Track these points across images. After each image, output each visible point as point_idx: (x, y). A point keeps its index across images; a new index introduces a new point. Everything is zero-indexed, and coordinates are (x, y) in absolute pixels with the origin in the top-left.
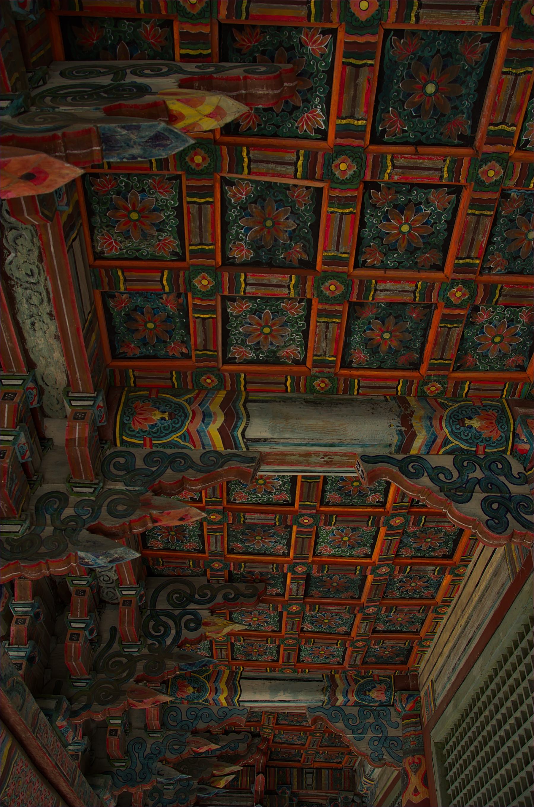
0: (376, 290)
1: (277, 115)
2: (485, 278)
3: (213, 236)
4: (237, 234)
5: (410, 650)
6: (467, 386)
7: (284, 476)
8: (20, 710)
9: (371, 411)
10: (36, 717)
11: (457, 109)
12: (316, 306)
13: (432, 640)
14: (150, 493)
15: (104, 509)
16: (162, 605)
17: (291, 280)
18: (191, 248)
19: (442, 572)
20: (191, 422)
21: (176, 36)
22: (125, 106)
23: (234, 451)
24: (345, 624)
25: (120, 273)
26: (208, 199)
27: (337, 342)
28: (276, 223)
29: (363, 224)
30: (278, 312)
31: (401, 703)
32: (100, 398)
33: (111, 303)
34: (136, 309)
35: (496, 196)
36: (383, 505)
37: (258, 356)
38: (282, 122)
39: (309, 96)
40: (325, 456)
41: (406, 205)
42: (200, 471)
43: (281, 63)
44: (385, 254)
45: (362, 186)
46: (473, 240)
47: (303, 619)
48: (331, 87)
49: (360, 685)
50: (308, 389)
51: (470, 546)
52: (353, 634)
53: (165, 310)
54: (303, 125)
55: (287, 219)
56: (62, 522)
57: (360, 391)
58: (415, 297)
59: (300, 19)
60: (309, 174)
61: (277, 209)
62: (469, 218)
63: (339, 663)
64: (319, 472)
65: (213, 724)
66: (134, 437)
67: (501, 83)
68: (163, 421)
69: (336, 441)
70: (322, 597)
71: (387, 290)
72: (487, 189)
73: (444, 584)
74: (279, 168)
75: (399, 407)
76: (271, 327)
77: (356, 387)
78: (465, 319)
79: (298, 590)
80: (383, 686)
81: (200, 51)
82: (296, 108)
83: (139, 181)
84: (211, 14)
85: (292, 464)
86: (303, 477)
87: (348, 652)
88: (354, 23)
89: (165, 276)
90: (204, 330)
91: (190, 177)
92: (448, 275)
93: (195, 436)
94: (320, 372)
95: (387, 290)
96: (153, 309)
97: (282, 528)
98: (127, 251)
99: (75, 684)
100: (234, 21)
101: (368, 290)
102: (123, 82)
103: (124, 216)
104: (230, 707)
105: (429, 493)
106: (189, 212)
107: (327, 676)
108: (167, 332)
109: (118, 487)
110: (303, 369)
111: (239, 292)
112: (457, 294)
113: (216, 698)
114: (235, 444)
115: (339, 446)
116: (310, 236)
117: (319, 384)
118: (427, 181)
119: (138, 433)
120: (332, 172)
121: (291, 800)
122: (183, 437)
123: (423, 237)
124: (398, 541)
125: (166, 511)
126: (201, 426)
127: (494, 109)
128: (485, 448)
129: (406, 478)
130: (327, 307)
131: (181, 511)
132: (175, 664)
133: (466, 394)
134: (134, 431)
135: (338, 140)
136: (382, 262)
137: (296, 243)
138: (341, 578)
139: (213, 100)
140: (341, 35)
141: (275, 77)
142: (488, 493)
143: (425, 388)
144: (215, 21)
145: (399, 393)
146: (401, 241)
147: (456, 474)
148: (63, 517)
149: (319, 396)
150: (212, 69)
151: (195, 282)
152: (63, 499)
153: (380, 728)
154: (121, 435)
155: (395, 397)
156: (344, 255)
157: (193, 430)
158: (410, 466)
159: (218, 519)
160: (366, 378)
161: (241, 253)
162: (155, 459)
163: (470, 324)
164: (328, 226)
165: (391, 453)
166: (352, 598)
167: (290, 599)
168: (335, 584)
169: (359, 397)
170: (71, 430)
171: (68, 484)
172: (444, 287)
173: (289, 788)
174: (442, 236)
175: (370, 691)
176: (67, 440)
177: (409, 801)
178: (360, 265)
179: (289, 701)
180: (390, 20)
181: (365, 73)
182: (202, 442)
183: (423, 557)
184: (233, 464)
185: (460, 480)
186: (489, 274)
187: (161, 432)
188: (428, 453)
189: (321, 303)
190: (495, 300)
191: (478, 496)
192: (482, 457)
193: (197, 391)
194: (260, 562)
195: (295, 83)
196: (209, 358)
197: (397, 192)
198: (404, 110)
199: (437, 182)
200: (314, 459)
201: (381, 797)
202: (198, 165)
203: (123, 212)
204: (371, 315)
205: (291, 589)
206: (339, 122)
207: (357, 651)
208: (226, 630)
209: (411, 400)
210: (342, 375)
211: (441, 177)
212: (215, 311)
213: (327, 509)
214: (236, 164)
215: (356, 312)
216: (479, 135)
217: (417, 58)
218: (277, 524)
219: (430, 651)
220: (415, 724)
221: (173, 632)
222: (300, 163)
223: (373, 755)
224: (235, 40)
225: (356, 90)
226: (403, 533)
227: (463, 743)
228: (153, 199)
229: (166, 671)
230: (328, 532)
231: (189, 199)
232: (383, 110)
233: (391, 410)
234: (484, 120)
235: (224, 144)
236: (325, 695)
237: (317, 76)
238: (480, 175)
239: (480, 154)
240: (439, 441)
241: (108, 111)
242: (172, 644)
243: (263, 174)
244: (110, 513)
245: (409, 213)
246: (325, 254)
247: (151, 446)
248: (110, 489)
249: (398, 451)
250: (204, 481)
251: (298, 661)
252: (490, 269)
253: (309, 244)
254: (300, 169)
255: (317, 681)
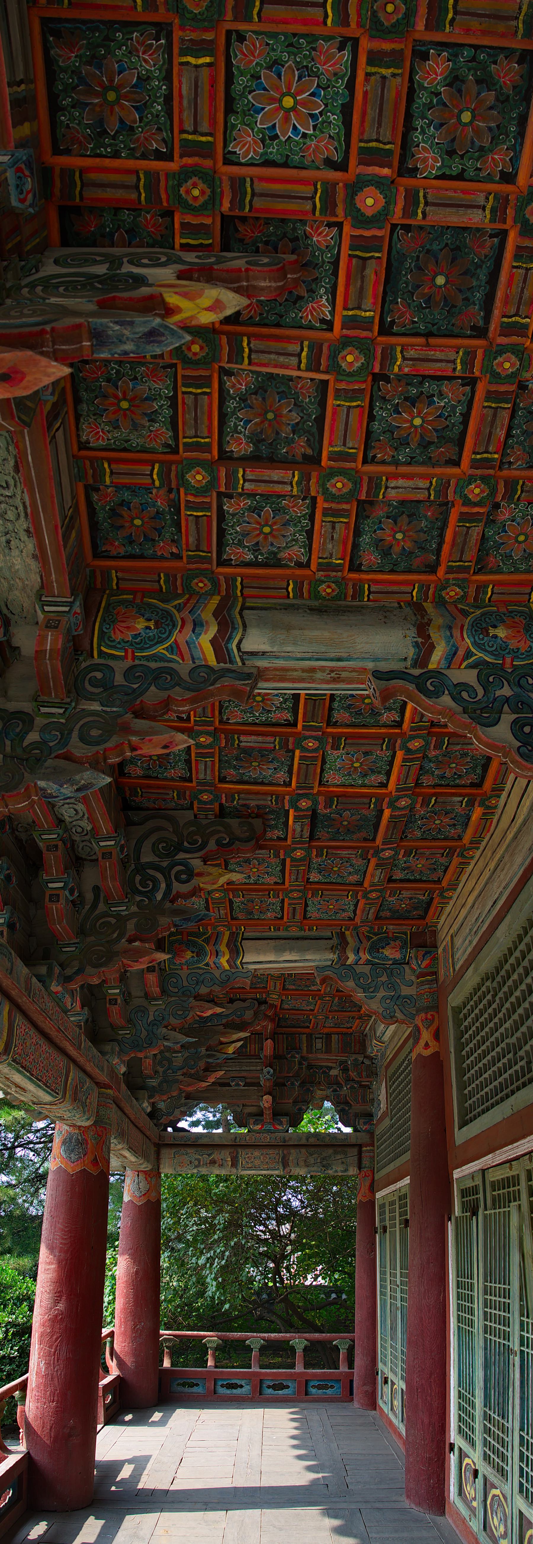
0: (387, 488)
1: (281, 305)
2: (505, 473)
3: (210, 430)
4: (236, 426)
5: (429, 903)
6: (490, 589)
7: (285, 694)
8: (11, 973)
9: (383, 620)
10: (28, 982)
11: (469, 301)
12: (321, 504)
13: (455, 890)
14: (129, 715)
15: (75, 734)
16: (147, 857)
17: (294, 476)
18: (185, 440)
19: (471, 804)
20: (180, 631)
21: (177, 226)
22: (120, 298)
23: (228, 665)
24: (357, 872)
25: (106, 465)
26: (205, 390)
27: (345, 544)
28: (278, 416)
29: (371, 418)
30: (279, 511)
31: (416, 959)
32: (78, 603)
33: (95, 497)
34: (122, 503)
35: (513, 388)
36: (399, 724)
37: (256, 557)
38: (285, 311)
39: (314, 286)
40: (332, 671)
41: (418, 398)
42: (189, 689)
43: (284, 253)
44: (396, 449)
45: (370, 378)
46: (490, 433)
47: (309, 867)
48: (337, 278)
49: (373, 942)
50: (312, 595)
51: (502, 772)
52: (366, 884)
53: (154, 506)
54: (307, 315)
55: (290, 411)
56: (24, 750)
57: (371, 597)
58: (430, 495)
59: (306, 213)
60: (313, 366)
61: (279, 401)
62: (485, 411)
63: (350, 919)
64: (324, 689)
65: (216, 988)
66: (114, 647)
67: (512, 276)
68: (148, 631)
69: (345, 655)
70: (330, 840)
71: (399, 488)
72: (503, 381)
73: (473, 818)
74: (281, 359)
75: (415, 615)
76: (271, 526)
77: (367, 593)
78: (485, 517)
79: (302, 831)
80: (398, 942)
81: (201, 241)
82: (300, 298)
83: (131, 369)
84: (214, 206)
85: (293, 681)
86: (307, 694)
87: (361, 905)
88: (360, 218)
89: (156, 470)
90: (198, 529)
91: (186, 366)
92: (465, 470)
93: (184, 648)
94: (325, 576)
95: (399, 488)
96: (141, 504)
97: (283, 752)
98: (115, 442)
99: (64, 950)
100: (237, 212)
101: (378, 487)
102: (118, 272)
103: (113, 404)
104: (233, 971)
105: (452, 714)
106: (184, 403)
107: (337, 933)
108: (156, 529)
109: (92, 708)
110: (307, 572)
111: (237, 488)
112: (476, 491)
113: (217, 961)
114: (230, 658)
115: (348, 659)
116: (314, 430)
117: (325, 590)
118: (439, 373)
119: (119, 643)
120: (338, 364)
121: (300, 1063)
122: (170, 649)
123: (436, 431)
124: (418, 767)
125: (147, 738)
126: (191, 637)
127: (506, 301)
128: (512, 661)
129: (423, 697)
130: (334, 506)
131: (165, 737)
132: (169, 920)
133: (490, 599)
134: (114, 641)
135: (345, 332)
136: (393, 457)
137: (299, 437)
138: (352, 815)
139: (212, 293)
140: (346, 228)
141: (278, 270)
142: (518, 713)
143: (443, 593)
144: (217, 212)
145: (415, 599)
146: (413, 435)
147: (481, 692)
148: (25, 744)
149: (325, 603)
150: (213, 260)
151: (188, 476)
152: (26, 720)
153: (393, 986)
154: (99, 645)
155: (410, 603)
156: (351, 451)
157: (181, 641)
158: (428, 683)
159: (208, 742)
160: (377, 582)
161: (240, 446)
162: (137, 674)
163: (490, 522)
164: (334, 420)
165: (406, 668)
166: (366, 840)
167: (293, 843)
168: (345, 823)
169: (370, 603)
170: (42, 639)
171: (34, 704)
172: (461, 483)
173: (298, 1053)
174: (458, 429)
175: (383, 948)
176: (36, 652)
177: (419, 1055)
178: (369, 460)
179: (296, 961)
180: (397, 215)
181: (371, 266)
182: (192, 655)
183: (448, 785)
184: (226, 681)
185: (485, 698)
186: (509, 469)
187: (145, 643)
188: (449, 667)
189: (326, 501)
190: (517, 496)
191: (508, 718)
192: (510, 671)
193: (187, 596)
194: (257, 793)
195: (298, 275)
196: (202, 560)
197: (408, 384)
198: (414, 301)
199: (450, 374)
200: (319, 675)
201: (391, 1056)
202: (195, 354)
203: (112, 400)
204: (381, 513)
205: (294, 830)
206: (345, 313)
207: (369, 904)
208: (222, 880)
209: (428, 606)
210: (350, 579)
211: (455, 369)
212: (209, 509)
213: (335, 730)
214: (236, 354)
215: (365, 511)
216: (492, 327)
217: (425, 251)
218: (277, 747)
219: (452, 903)
220: (430, 982)
221: (163, 886)
222: (304, 354)
223: (385, 1013)
224: (237, 231)
225: (362, 282)
226: (423, 758)
227: (481, 1006)
228: (145, 388)
229: (159, 928)
230: (336, 757)
231: (184, 389)
232: (391, 302)
233: (405, 619)
234: (496, 312)
235: (223, 333)
236: (335, 953)
237: (322, 267)
238: (495, 367)
239: (494, 346)
240: (461, 653)
241: (101, 304)
242: (163, 898)
243: (264, 365)
244: (82, 739)
245: (421, 405)
246: (331, 449)
247: (133, 659)
248: (84, 710)
249: (414, 666)
250: (192, 700)
251: (305, 918)
252: (510, 463)
253: (314, 437)
254: (304, 361)
255: (326, 939)
